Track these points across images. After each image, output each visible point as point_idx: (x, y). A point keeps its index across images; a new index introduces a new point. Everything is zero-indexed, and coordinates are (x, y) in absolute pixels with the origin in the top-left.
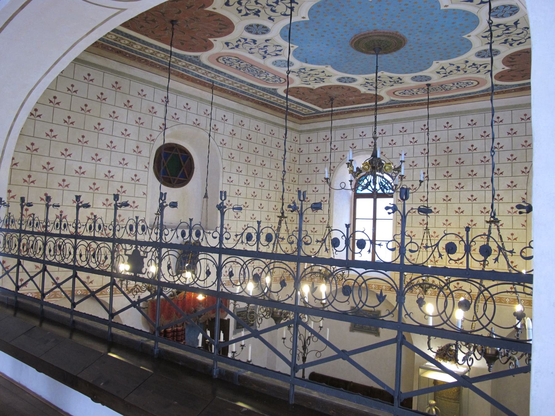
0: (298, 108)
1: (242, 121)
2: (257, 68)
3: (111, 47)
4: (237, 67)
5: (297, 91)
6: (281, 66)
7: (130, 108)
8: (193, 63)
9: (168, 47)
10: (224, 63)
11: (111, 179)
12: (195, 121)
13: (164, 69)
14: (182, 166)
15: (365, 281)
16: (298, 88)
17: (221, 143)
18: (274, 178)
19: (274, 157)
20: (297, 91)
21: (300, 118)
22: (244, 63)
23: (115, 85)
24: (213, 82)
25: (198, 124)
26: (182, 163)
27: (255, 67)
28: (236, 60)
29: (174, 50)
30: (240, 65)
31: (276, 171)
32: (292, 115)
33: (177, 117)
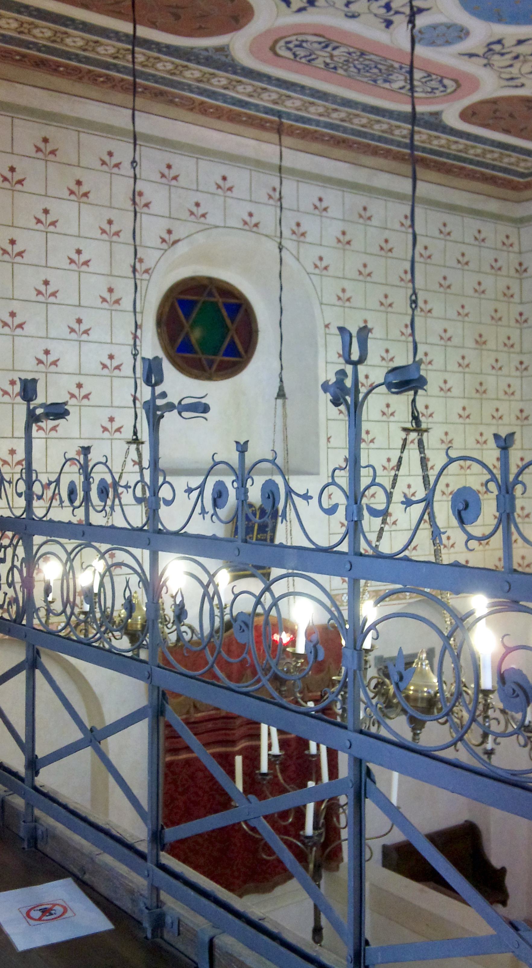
0: (506, 160)
1: (365, 209)
3: (18, 53)
4: (327, 64)
6: (438, 42)
7: (84, 199)
8: (218, 68)
9: (126, 27)
10: (292, 57)
11: (53, 368)
12: (247, 219)
13: (156, 95)
15: (275, 604)
16: (494, 101)
17: (316, 266)
18: (456, 341)
19: (453, 289)
20: (495, 111)
21: (515, 187)
22: (342, 49)
23: (42, 145)
24: (279, 114)
25: (256, 225)
26: (228, 321)
27: (373, 57)
28: (320, 43)
29: (143, 32)
30: (332, 57)
31: (460, 324)
33: (201, 211)
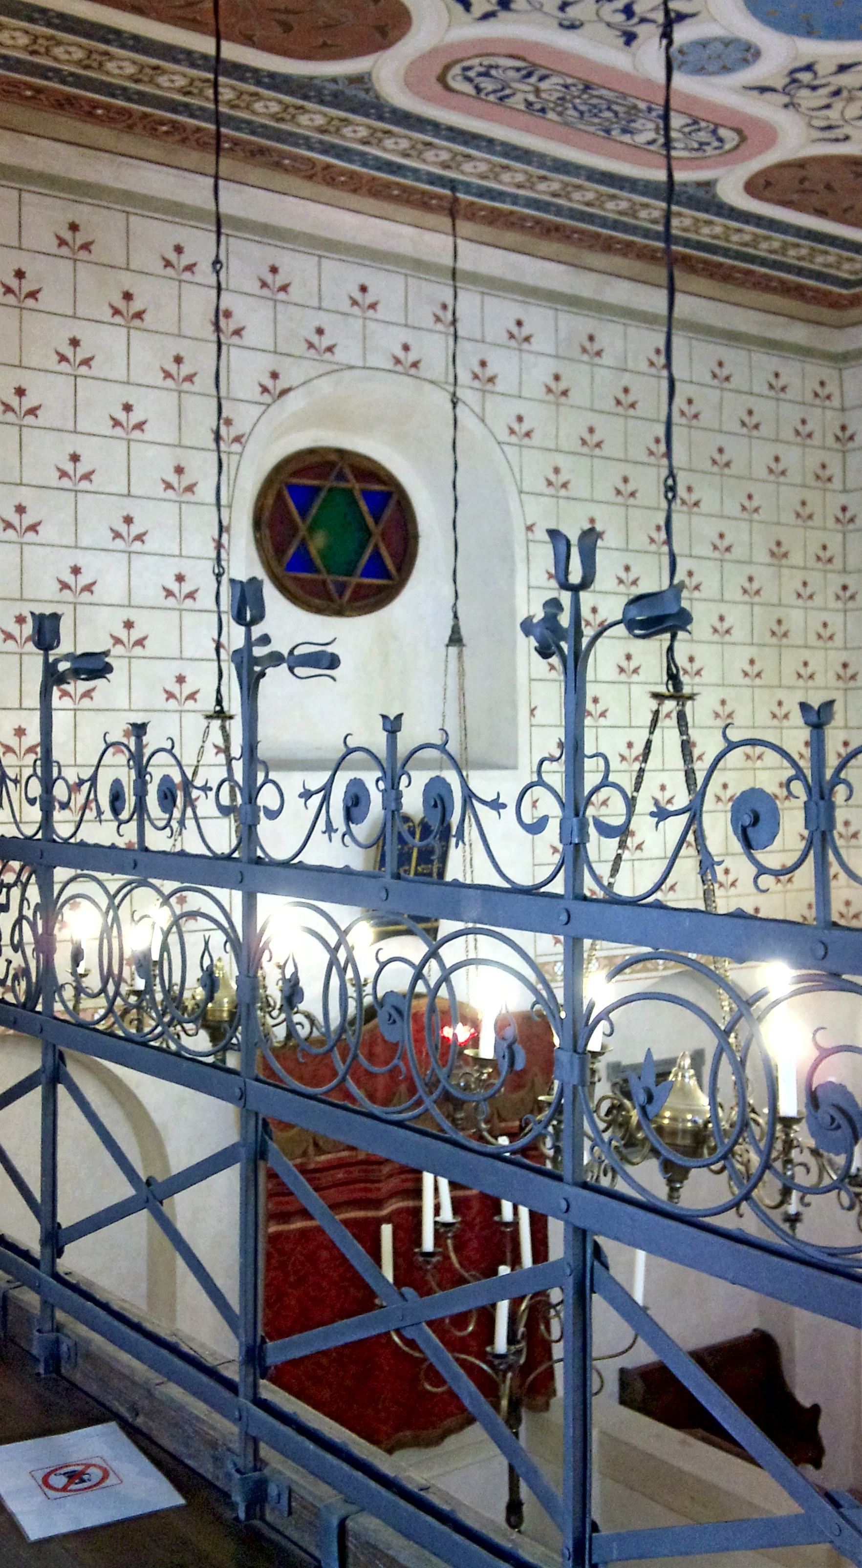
0: (820, 259)
1: (591, 338)
2: (610, 95)
4: (529, 104)
5: (802, 180)
6: (710, 68)
7: (137, 323)
9: (204, 44)
10: (473, 92)
11: (86, 597)
12: (401, 354)
14: (370, 534)
16: (801, 164)
17: (512, 432)
18: (738, 552)
20: (802, 180)
21: (835, 304)
22: (555, 80)
23: (67, 235)
24: (453, 185)
25: (415, 365)
26: (370, 520)
27: (603, 92)
28: (518, 70)
29: (232, 52)
30: (537, 92)
31: (745, 526)
32: (686, 262)
33: (326, 342)
